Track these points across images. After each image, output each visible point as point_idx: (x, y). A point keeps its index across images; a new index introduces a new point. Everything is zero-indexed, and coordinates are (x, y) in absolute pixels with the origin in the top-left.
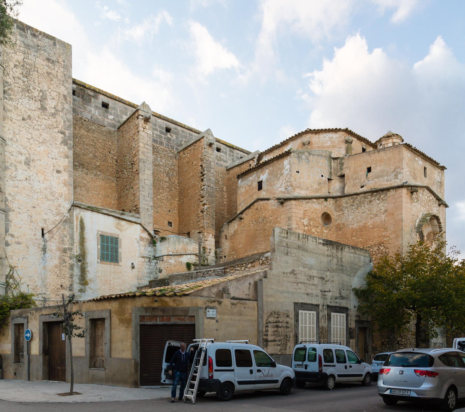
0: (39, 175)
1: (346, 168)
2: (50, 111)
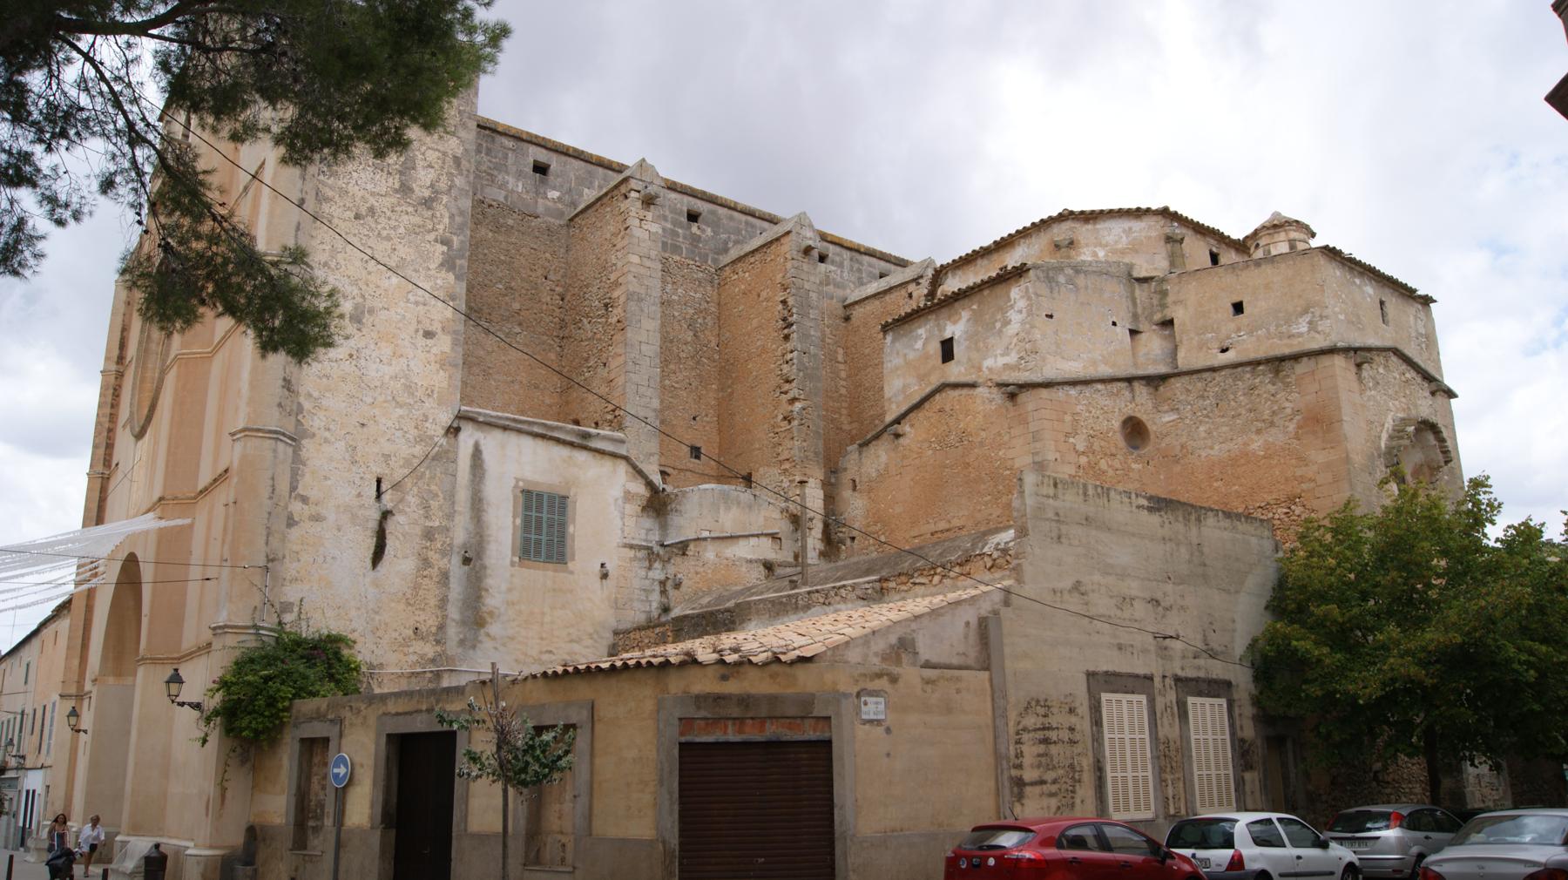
0: (382, 344)
1: (1175, 303)
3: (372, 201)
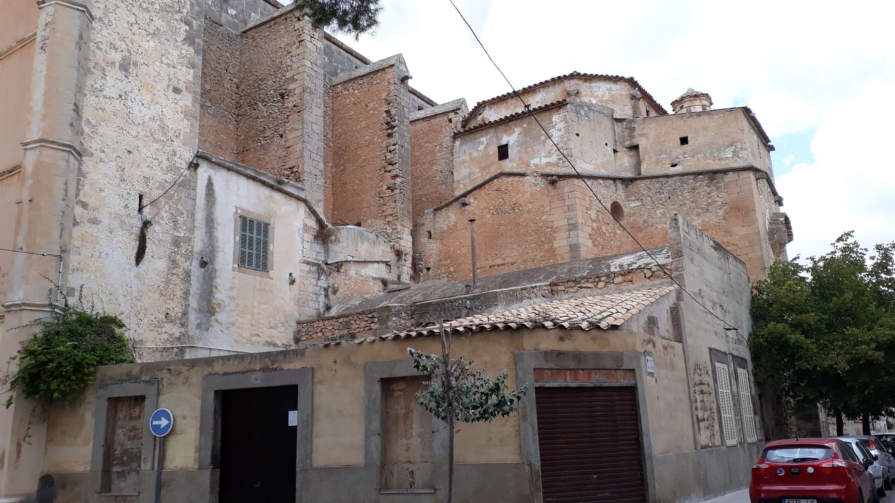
1: (640, 135)
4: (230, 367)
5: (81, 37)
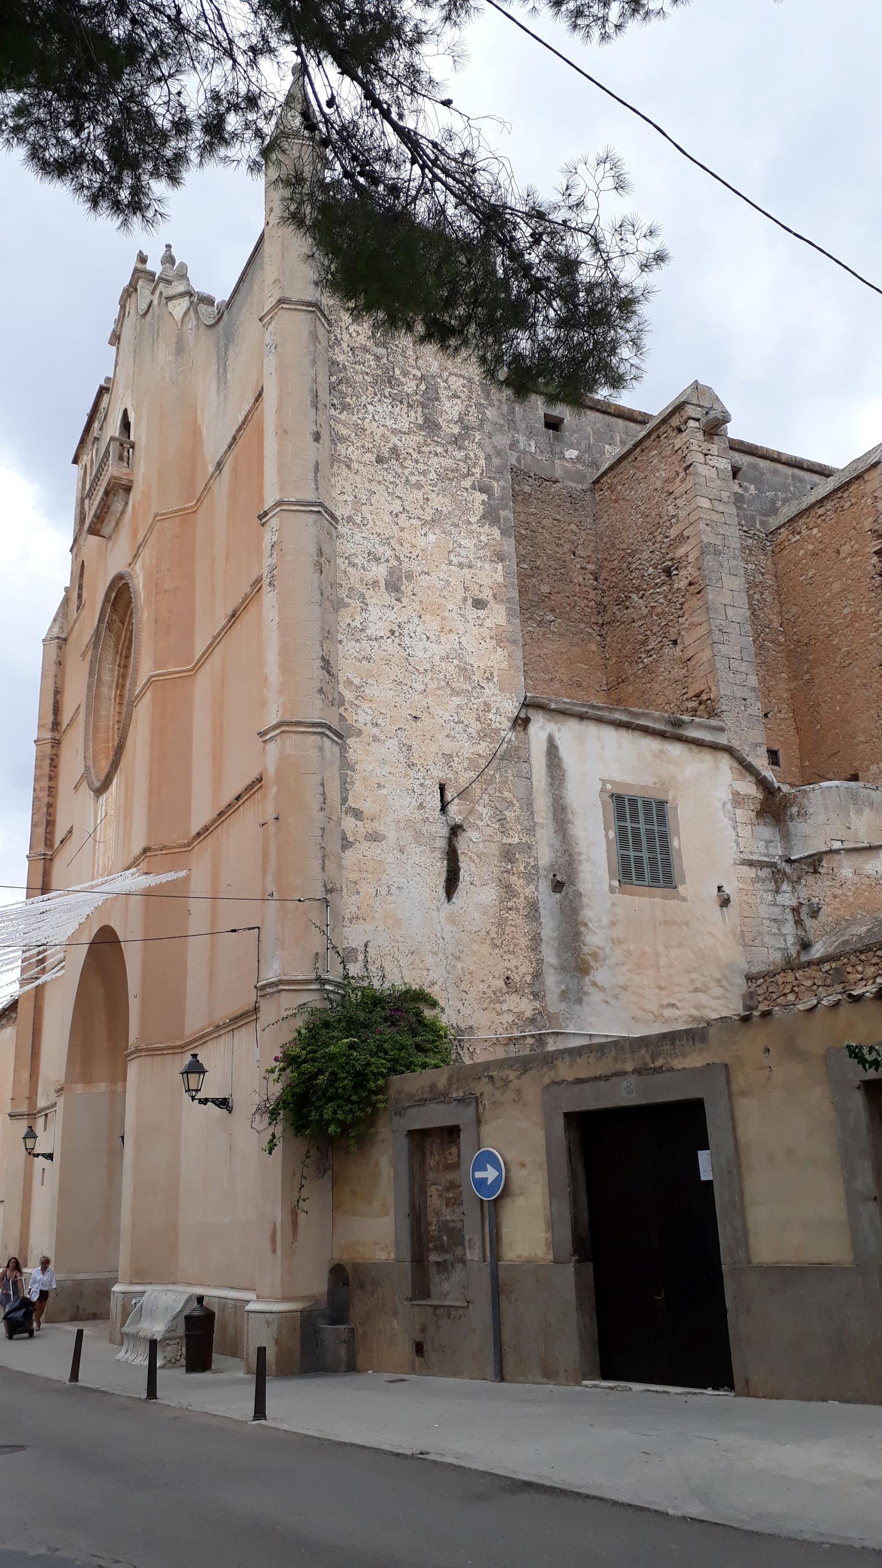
0: (427, 617)
2: (448, 431)
3: (394, 440)
4: (583, 1069)
5: (320, 553)
